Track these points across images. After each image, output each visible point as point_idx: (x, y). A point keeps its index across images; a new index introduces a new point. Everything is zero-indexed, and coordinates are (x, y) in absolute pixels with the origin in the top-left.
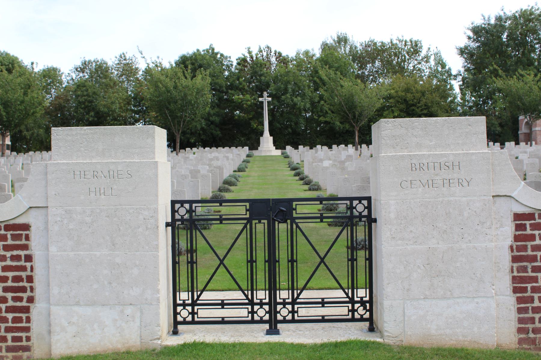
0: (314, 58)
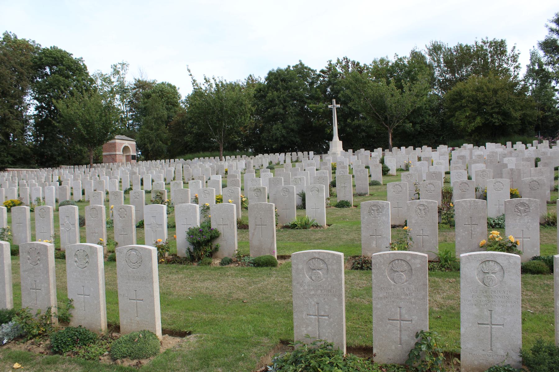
0: (390, 64)
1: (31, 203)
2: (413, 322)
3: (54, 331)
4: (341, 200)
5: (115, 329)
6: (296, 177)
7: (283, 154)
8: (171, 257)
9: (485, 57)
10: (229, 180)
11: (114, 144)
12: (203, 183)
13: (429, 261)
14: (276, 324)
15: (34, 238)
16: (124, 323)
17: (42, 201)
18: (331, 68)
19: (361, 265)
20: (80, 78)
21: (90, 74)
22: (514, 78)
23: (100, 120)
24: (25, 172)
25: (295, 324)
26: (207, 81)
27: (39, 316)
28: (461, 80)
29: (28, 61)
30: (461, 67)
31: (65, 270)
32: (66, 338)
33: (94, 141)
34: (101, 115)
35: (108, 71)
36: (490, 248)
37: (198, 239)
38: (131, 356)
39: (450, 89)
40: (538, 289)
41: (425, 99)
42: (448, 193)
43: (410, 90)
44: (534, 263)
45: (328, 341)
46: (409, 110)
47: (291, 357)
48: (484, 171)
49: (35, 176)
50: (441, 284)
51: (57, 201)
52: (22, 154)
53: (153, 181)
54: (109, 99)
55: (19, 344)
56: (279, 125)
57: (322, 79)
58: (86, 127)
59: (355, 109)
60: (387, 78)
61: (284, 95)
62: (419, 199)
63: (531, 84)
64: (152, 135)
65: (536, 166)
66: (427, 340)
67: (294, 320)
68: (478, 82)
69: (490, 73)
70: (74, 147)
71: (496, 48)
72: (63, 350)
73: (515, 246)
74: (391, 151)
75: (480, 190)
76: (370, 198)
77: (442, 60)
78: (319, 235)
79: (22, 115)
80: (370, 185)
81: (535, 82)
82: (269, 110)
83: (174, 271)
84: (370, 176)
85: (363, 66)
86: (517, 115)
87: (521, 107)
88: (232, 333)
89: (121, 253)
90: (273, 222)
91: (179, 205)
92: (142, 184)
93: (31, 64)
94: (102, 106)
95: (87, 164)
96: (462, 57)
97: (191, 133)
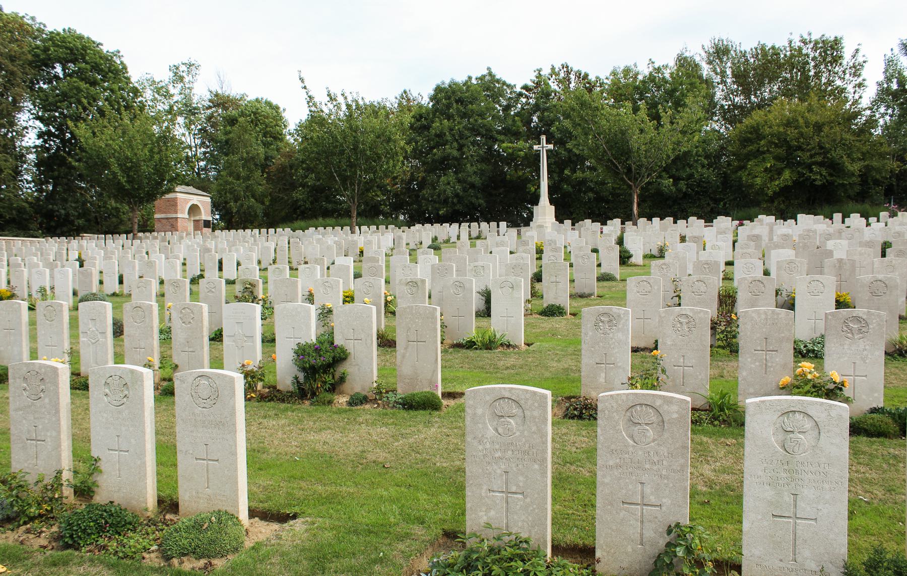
0: (640, 77)
1: (30, 296)
2: (664, 508)
3: (66, 511)
4: (550, 303)
5: (170, 507)
6: (476, 264)
7: (455, 226)
8: (267, 390)
9: (804, 68)
10: (365, 266)
11: (175, 200)
12: (322, 270)
13: (693, 409)
14: (437, 505)
15: (34, 354)
16: (185, 497)
17: (49, 292)
18: (540, 82)
19: (580, 411)
20: (115, 87)
21: (133, 80)
22: (853, 104)
23: (151, 160)
24: (19, 243)
25: (468, 506)
26: (332, 99)
27: (40, 485)
28: (760, 106)
29: (23, 53)
30: (761, 84)
31: (87, 409)
32: (90, 522)
33: (140, 194)
34: (151, 151)
35: (163, 76)
36: (797, 390)
37: (313, 362)
38: (195, 552)
39: (741, 122)
40: (877, 462)
41: (696, 138)
42: (730, 296)
43: (672, 123)
44: (873, 419)
45: (521, 535)
46: (668, 157)
47: (460, 560)
48: (791, 262)
49: (37, 250)
50: (712, 447)
51: (75, 294)
52: (14, 212)
53: (238, 264)
54: (166, 124)
55: (5, 532)
56: (451, 176)
57: (524, 100)
58: (126, 170)
59: (577, 152)
60: (634, 102)
61: (461, 126)
62: (679, 305)
63: (883, 116)
64: (239, 187)
65: (884, 255)
66: (685, 539)
67: (467, 499)
68: (790, 111)
69: (812, 94)
70: (105, 203)
71: (825, 52)
72: (80, 542)
73: (841, 389)
74: (635, 224)
75: (784, 293)
76: (598, 301)
77: (729, 72)
78: (511, 361)
79: (14, 145)
80: (599, 279)
81: (890, 111)
82: (435, 150)
83: (271, 413)
84: (599, 265)
85: (593, 79)
86: (855, 167)
87: (863, 154)
88: (364, 517)
89: (183, 381)
90: (436, 336)
91: (283, 305)
92: (220, 269)
93: (30, 57)
94: (154, 135)
95: (127, 233)
96: (765, 67)
97: (304, 185)
